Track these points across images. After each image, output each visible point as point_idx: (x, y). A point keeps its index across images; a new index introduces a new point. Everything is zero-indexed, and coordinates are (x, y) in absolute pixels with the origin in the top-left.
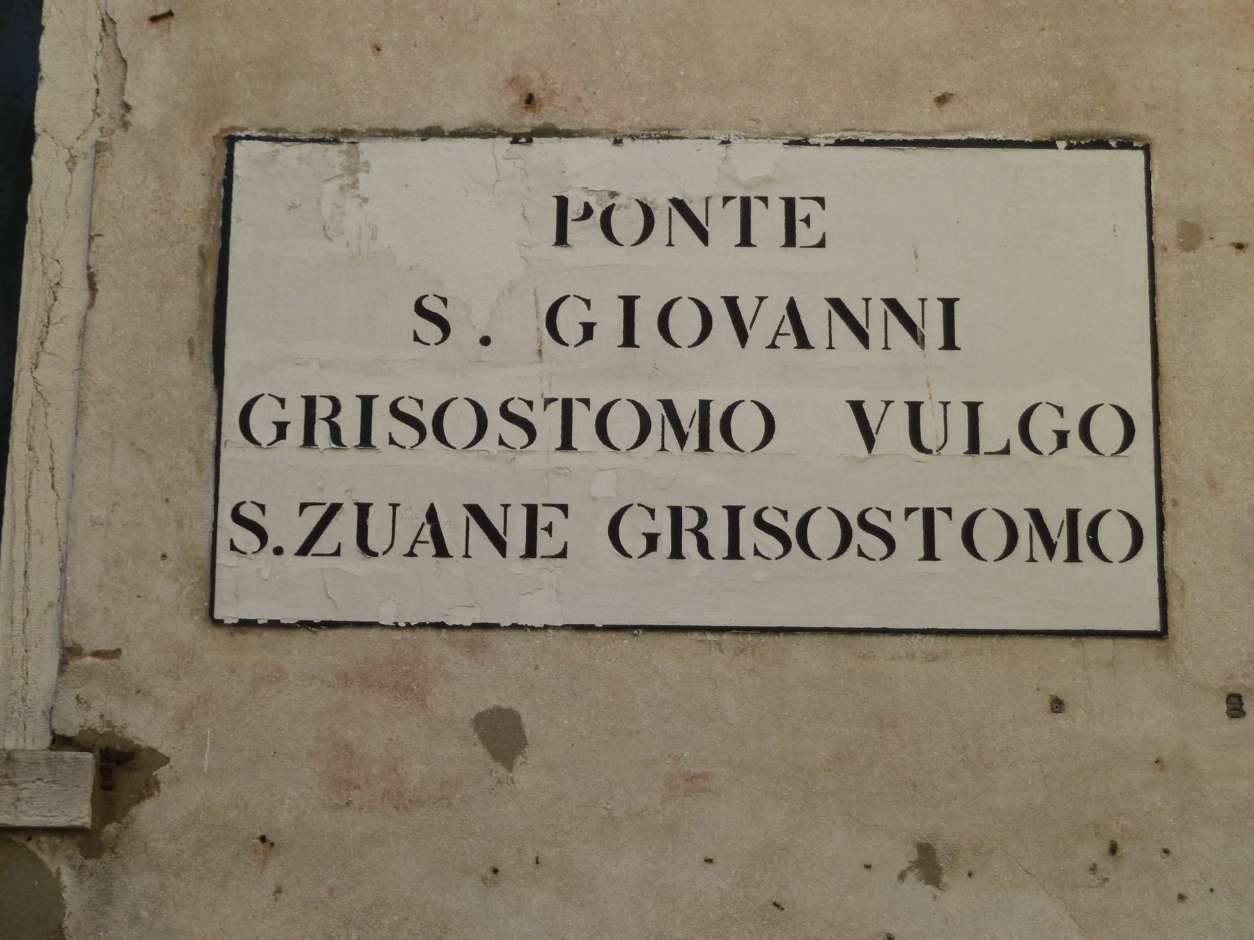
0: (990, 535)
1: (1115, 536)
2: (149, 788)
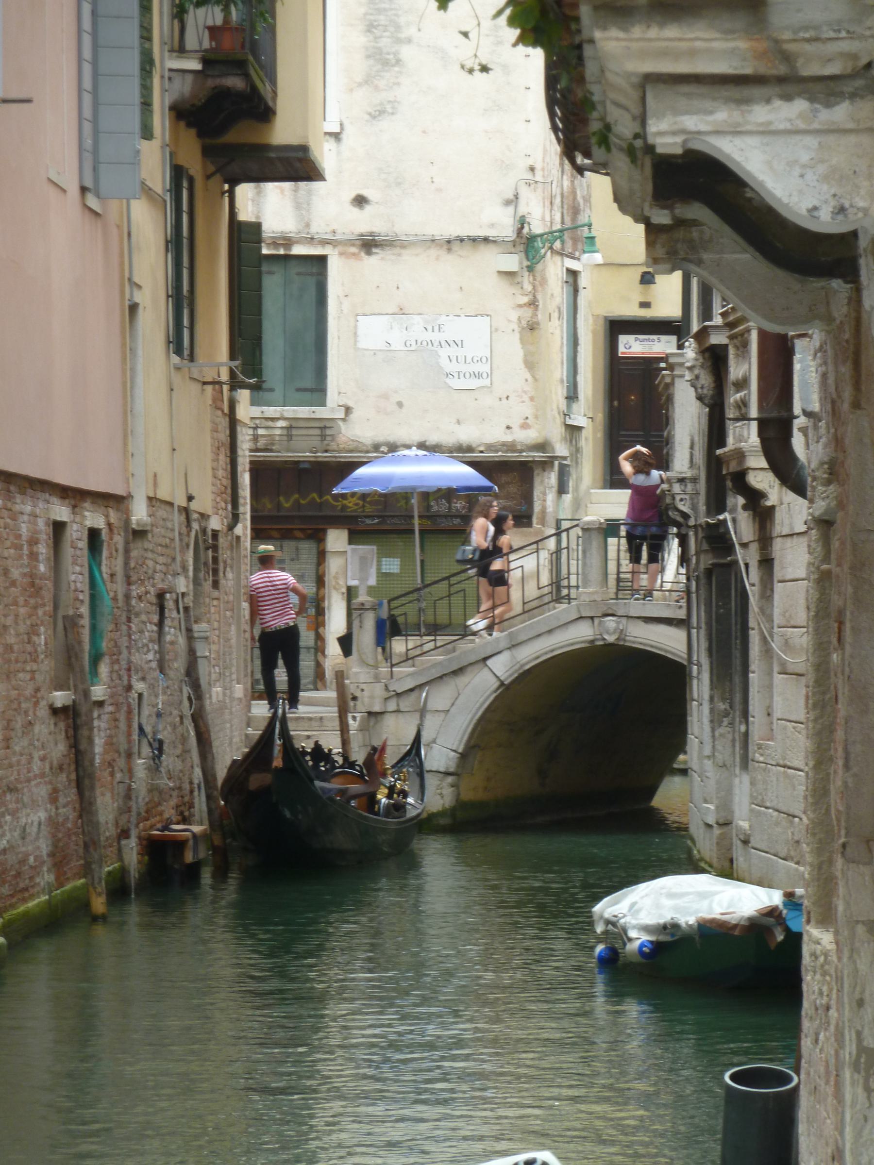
0: (467, 375)
1: (485, 375)
2: (352, 413)
